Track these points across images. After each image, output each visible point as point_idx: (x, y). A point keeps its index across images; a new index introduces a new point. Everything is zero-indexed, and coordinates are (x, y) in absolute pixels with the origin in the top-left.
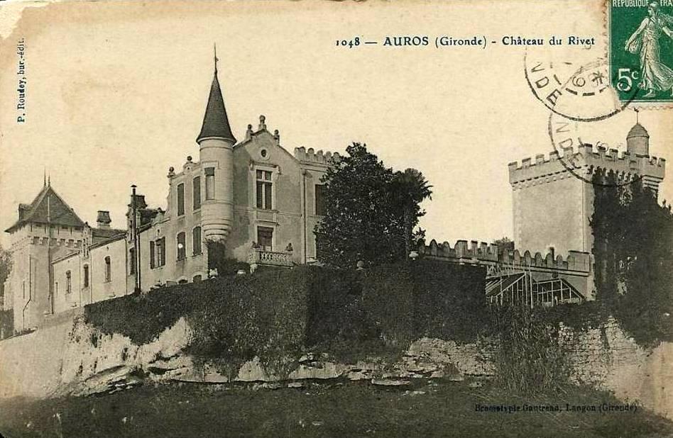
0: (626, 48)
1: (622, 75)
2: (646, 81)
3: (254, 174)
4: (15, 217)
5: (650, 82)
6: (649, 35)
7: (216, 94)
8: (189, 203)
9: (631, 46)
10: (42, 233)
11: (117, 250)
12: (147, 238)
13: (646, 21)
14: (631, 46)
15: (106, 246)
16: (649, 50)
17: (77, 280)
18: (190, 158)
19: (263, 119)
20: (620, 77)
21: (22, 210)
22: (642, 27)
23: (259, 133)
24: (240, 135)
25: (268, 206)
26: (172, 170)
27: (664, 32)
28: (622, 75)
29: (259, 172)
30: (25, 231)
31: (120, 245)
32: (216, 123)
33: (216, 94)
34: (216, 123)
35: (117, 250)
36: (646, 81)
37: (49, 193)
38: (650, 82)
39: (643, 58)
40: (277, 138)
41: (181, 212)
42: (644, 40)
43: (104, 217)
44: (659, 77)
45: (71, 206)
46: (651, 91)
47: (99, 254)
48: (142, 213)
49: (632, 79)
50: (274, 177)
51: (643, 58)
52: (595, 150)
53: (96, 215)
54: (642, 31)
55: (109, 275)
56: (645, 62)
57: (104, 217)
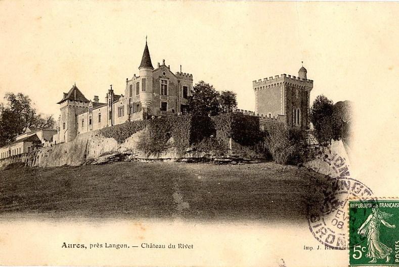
0: (358, 233)
1: (356, 249)
2: (371, 253)
3: (160, 81)
4: (62, 97)
5: (373, 253)
6: (372, 225)
7: (147, 51)
8: (134, 92)
9: (362, 231)
10: (72, 103)
11: (104, 111)
12: (116, 105)
13: (371, 216)
14: (362, 231)
15: (99, 109)
16: (373, 235)
17: (86, 122)
18: (135, 75)
19: (164, 61)
20: (355, 251)
21: (66, 95)
22: (368, 220)
23: (164, 68)
24: (155, 66)
25: (166, 94)
26: (127, 79)
27: (382, 223)
28: (356, 249)
29: (163, 81)
30: (66, 103)
31: (104, 108)
32: (147, 61)
33: (147, 51)
34: (147, 61)
35: (104, 111)
36: (371, 253)
37: (75, 88)
38: (373, 253)
39: (369, 239)
40: (169, 68)
41: (131, 95)
42: (370, 228)
43: (96, 98)
44: (379, 250)
45: (83, 94)
46: (374, 259)
47: (96, 112)
48: (114, 98)
49: (362, 251)
50: (168, 83)
51: (369, 239)
52: (287, 76)
53: (93, 98)
54: (369, 222)
55: (100, 120)
56: (370, 242)
57: (96, 98)
